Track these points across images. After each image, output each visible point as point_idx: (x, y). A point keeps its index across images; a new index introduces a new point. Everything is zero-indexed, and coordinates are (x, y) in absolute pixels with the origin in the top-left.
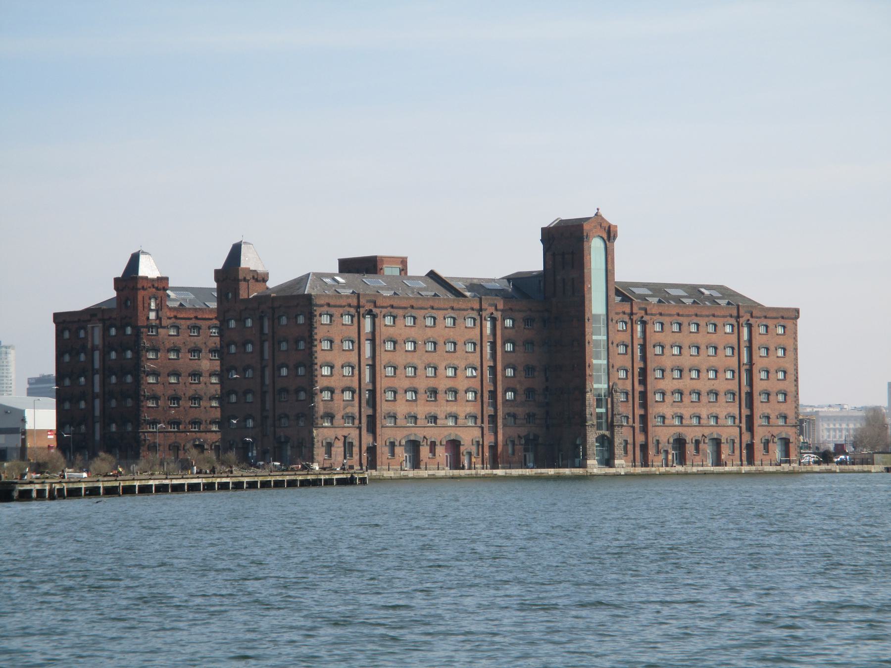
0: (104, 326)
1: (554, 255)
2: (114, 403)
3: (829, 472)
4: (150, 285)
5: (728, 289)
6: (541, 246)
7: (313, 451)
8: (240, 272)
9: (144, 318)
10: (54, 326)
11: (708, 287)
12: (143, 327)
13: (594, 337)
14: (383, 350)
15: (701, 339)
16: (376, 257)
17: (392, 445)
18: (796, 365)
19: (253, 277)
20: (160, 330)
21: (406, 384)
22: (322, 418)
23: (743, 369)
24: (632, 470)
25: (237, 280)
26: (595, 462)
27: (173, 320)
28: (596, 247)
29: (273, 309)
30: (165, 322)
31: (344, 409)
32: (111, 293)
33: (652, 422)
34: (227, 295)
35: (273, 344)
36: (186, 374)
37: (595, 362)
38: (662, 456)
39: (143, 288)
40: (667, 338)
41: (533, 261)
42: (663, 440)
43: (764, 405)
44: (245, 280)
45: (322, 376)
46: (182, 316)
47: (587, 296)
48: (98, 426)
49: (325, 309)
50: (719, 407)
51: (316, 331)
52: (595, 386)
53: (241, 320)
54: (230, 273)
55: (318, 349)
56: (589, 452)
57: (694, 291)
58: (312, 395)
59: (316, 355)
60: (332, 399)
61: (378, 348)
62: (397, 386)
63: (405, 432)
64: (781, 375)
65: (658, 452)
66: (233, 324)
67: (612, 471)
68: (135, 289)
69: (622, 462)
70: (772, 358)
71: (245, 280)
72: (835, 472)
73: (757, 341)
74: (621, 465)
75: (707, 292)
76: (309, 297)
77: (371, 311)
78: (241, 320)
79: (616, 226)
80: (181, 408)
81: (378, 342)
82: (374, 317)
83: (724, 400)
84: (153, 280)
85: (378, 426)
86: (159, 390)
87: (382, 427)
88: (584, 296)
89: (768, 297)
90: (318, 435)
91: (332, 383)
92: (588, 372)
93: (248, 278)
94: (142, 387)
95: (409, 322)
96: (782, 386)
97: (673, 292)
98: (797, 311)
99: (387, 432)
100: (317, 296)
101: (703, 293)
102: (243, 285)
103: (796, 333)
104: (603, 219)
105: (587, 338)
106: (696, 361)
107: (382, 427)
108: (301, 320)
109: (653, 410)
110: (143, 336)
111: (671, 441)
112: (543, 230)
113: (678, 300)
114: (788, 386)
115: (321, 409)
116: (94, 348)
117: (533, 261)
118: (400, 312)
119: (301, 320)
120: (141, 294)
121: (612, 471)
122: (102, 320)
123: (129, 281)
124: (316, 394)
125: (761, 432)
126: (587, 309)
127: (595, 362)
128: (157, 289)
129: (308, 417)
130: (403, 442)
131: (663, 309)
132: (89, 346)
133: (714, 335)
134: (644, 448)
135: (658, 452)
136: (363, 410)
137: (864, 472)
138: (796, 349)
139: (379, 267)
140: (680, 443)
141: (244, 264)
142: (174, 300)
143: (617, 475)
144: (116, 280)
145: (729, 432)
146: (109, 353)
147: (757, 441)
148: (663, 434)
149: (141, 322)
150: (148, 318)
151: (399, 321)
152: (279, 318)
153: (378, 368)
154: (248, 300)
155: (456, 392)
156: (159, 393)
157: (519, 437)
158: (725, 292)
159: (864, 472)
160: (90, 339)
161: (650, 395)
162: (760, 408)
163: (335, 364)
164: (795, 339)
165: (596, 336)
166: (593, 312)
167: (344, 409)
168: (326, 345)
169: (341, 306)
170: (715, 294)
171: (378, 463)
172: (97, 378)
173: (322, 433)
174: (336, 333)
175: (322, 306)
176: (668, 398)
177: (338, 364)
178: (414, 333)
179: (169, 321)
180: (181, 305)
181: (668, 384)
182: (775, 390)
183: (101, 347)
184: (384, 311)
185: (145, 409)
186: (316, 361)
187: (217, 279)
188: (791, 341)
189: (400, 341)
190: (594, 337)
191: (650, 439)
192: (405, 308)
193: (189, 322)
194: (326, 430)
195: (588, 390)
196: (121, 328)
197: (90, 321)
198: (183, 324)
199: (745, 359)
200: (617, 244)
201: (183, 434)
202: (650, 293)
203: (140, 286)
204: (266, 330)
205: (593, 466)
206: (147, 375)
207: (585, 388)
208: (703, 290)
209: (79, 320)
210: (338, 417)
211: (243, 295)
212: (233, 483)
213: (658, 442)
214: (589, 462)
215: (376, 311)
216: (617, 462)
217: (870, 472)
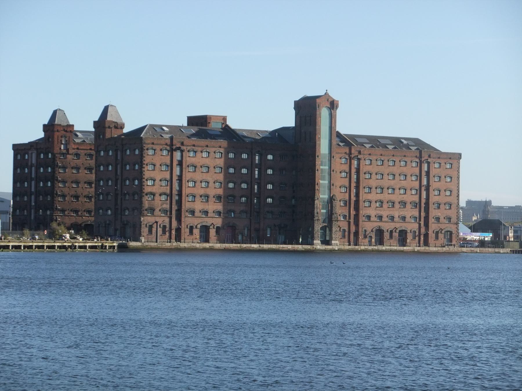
0: (37, 152)
1: (301, 117)
2: (41, 198)
3: (472, 252)
4: (62, 129)
5: (420, 140)
6: (294, 112)
7: (141, 229)
8: (106, 123)
9: (58, 149)
10: (13, 151)
11: (167, 126)
12: (57, 154)
13: (321, 167)
14: (187, 171)
15: (396, 170)
16: (206, 116)
17: (191, 228)
18: (458, 187)
19: (115, 126)
20: (68, 156)
21: (202, 192)
22: (146, 210)
23: (423, 188)
24: (342, 247)
25: (105, 128)
26: (319, 242)
27: (76, 150)
28: (324, 113)
29: (123, 145)
30: (71, 151)
31: (161, 205)
32: (41, 135)
33: (361, 219)
34: (100, 136)
35: (122, 166)
36: (77, 181)
37: (321, 182)
38: (367, 240)
39: (58, 131)
40: (373, 169)
41: (289, 120)
42: (369, 230)
43: (437, 210)
44: (109, 127)
45: (148, 185)
46: (82, 148)
47: (317, 142)
48: (33, 211)
49: (150, 146)
50: (407, 211)
51: (144, 159)
52: (321, 196)
53: (106, 151)
54: (101, 124)
55: (145, 169)
56: (316, 236)
57: (193, 126)
58: (141, 197)
59: (144, 173)
60: (153, 199)
61: (184, 170)
62: (209, 194)
63: (200, 220)
64: (448, 193)
65: (365, 237)
66: (102, 153)
67: (329, 247)
68: (53, 131)
69: (337, 242)
70: (443, 182)
71: (109, 127)
72: (477, 252)
73: (363, 169)
74: (336, 244)
75: (405, 142)
76: (142, 137)
77: (180, 148)
78: (106, 151)
79: (338, 101)
80: (80, 202)
81: (184, 166)
82: (182, 151)
83: (410, 207)
84: (64, 126)
85: (183, 216)
86: (66, 191)
87: (185, 217)
88: (315, 143)
89: (443, 146)
90: (144, 220)
91: (154, 190)
92: (317, 187)
93: (111, 126)
94: (56, 189)
95: (205, 155)
96: (448, 199)
97: (383, 141)
98: (460, 155)
99: (187, 220)
100: (146, 138)
101: (402, 143)
102: (108, 131)
103: (459, 168)
104: (329, 96)
105: (317, 167)
106: (392, 183)
107: (185, 217)
108: (137, 152)
109: (362, 212)
110: (57, 159)
111: (374, 230)
112: (295, 102)
113: (385, 146)
114: (452, 199)
115: (146, 205)
116: (32, 165)
117: (289, 120)
118: (200, 149)
119: (137, 152)
120: (56, 134)
121: (329, 247)
122: (37, 149)
123: (49, 128)
124: (143, 196)
125: (433, 226)
126: (317, 150)
127: (321, 182)
128: (66, 131)
129: (139, 209)
130: (199, 226)
131: (373, 151)
132: (30, 164)
133: (405, 168)
134: (356, 234)
135: (365, 237)
136: (173, 206)
137: (496, 253)
138: (458, 178)
139: (208, 121)
140: (380, 232)
141: (109, 118)
142: (80, 138)
143: (332, 251)
144: (44, 126)
145: (412, 226)
146: (40, 168)
147: (430, 232)
148: (368, 226)
149: (56, 150)
150: (60, 149)
151: (199, 154)
152: (126, 150)
153: (184, 182)
154: (112, 138)
155: (382, 202)
156: (66, 193)
157: (275, 225)
158: (417, 142)
159: (496, 253)
160: (30, 160)
161: (361, 203)
162: (433, 212)
163: (155, 177)
164: (458, 172)
165: (322, 167)
166: (322, 152)
167: (161, 205)
168: (150, 167)
169: (161, 145)
170: (411, 143)
171: (182, 238)
172: (33, 183)
173: (147, 220)
174: (157, 160)
175: (149, 144)
176: (373, 205)
177: (158, 179)
178: (208, 162)
179: (74, 151)
180: (84, 141)
181: (374, 196)
182: (444, 202)
183: (35, 165)
184: (189, 148)
185: (57, 202)
186: (144, 176)
187: (95, 127)
188: (456, 173)
189: (199, 166)
190: (321, 167)
191: (360, 230)
192: (202, 146)
193: (86, 152)
194: (149, 217)
195: (316, 198)
196: (46, 154)
197: (30, 149)
198: (82, 153)
199: (425, 182)
200: (339, 113)
201: (81, 218)
202: (368, 141)
203: (56, 129)
204: (119, 158)
205: (318, 245)
206: (59, 182)
207: (314, 197)
208: (403, 140)
209: (25, 149)
210: (157, 210)
211: (108, 136)
212: (109, 246)
213: (365, 231)
214: (315, 242)
215: (183, 148)
216: (333, 242)
217: (499, 253)
